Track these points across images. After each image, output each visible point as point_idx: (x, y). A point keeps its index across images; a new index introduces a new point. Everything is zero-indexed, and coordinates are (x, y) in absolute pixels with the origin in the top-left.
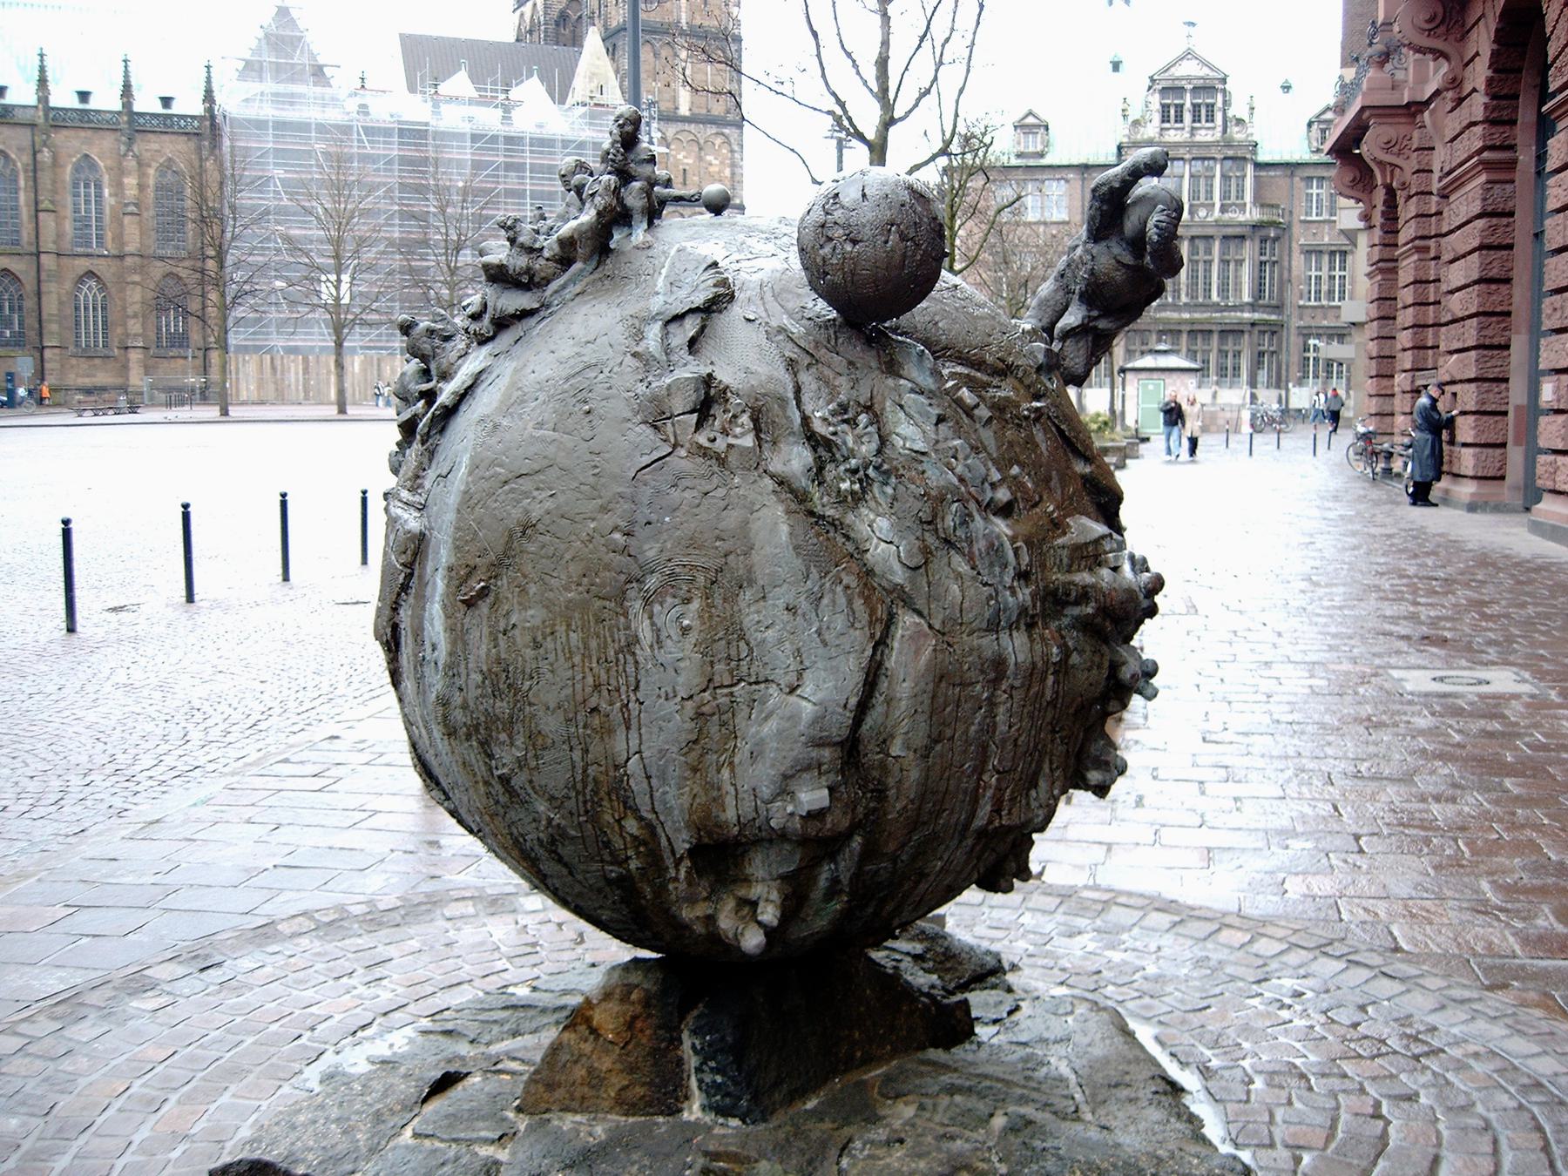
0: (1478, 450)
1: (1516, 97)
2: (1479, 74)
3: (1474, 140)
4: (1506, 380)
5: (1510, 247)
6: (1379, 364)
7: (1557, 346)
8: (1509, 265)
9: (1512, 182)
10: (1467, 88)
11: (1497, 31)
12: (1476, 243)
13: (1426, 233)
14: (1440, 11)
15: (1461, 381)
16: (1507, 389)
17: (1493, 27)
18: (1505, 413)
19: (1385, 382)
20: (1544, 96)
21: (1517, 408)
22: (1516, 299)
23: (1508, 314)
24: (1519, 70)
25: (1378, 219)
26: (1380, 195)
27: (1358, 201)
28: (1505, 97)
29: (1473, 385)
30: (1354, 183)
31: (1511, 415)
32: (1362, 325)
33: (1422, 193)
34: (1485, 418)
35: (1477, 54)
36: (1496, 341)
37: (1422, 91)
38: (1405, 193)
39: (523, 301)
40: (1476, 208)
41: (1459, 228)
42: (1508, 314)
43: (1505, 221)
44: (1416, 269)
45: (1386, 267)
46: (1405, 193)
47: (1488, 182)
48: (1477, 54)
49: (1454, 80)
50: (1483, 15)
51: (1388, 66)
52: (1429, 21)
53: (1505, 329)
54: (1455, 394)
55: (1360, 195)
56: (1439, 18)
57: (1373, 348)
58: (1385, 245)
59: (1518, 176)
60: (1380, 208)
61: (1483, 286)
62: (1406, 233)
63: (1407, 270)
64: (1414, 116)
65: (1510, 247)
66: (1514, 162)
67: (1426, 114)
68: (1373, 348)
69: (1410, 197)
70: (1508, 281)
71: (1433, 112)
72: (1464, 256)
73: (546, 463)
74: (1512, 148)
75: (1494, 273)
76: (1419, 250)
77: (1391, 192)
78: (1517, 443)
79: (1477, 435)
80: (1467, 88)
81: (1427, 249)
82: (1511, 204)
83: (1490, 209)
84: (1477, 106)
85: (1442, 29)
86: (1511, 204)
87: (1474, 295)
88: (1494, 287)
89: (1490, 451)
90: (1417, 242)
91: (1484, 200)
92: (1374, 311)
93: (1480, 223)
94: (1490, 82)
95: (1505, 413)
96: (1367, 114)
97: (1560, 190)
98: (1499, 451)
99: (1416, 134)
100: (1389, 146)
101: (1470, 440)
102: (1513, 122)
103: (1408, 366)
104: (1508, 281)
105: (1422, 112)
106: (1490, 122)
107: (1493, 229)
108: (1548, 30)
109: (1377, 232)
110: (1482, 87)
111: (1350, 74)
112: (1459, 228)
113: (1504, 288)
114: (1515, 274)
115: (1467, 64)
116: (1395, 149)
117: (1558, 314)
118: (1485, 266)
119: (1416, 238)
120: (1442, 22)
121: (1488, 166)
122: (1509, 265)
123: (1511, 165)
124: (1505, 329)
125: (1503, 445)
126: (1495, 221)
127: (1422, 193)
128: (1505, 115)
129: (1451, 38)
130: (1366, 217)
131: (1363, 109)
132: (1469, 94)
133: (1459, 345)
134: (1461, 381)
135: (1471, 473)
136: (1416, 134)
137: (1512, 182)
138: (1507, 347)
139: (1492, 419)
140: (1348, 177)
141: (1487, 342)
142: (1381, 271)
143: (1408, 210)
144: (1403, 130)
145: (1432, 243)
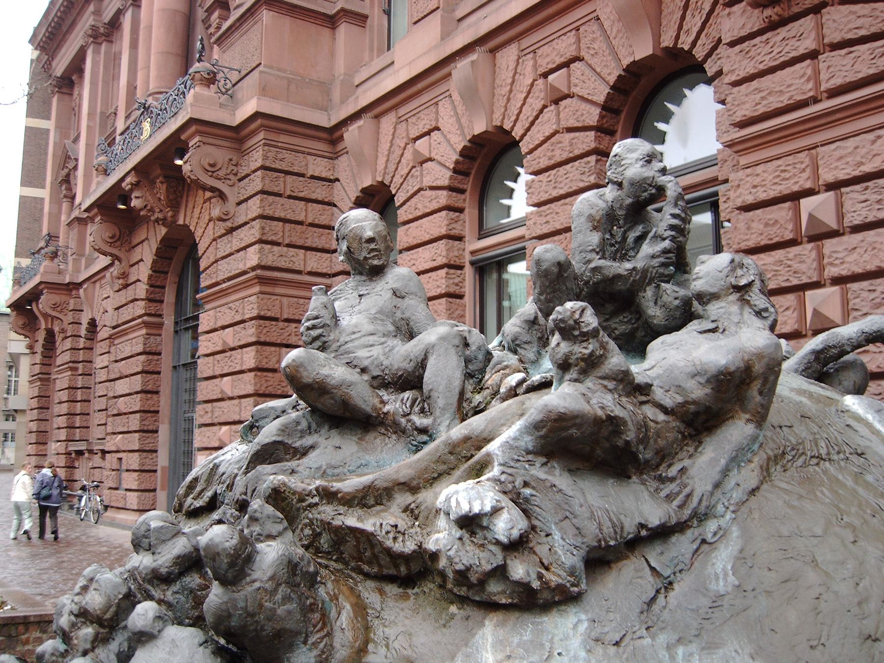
0: (140, 493)
1: (164, 287)
2: (143, 272)
3: (139, 308)
4: (156, 451)
5: (159, 373)
6: (37, 436)
7: (208, 434)
8: (158, 383)
9: (160, 335)
10: (132, 279)
11: (158, 248)
12: (139, 369)
13: (76, 359)
14: (118, 234)
15: (124, 451)
16: (157, 457)
17: (154, 247)
18: (155, 471)
19: (41, 447)
20: (197, 290)
21: (163, 468)
22: (162, 403)
23: (157, 412)
24: (167, 273)
25: (39, 348)
26: (41, 336)
27: (26, 336)
28: (158, 287)
29: (137, 454)
30: (24, 327)
31: (159, 472)
32: (23, 411)
33: (75, 336)
34: (144, 474)
35: (142, 260)
36: (150, 428)
37: (78, 277)
38: (62, 335)
39: (638, 504)
40: (140, 348)
41: (122, 359)
42: (157, 412)
43: (156, 357)
44: (70, 380)
45: (43, 378)
46: (62, 335)
47: (147, 334)
48: (142, 260)
49: (124, 273)
50: (147, 239)
51: (56, 260)
52: (111, 238)
53: (155, 421)
54: (120, 459)
55: (28, 334)
56: (117, 237)
57: (34, 426)
58: (43, 364)
59: (163, 333)
60: (41, 341)
61: (144, 395)
62: (62, 358)
63: (62, 380)
64: (71, 290)
65: (159, 373)
66: (162, 324)
67: (81, 291)
68: (34, 426)
69: (67, 337)
70: (157, 393)
71: (85, 290)
72: (127, 376)
73: (448, 625)
74: (160, 316)
75: (150, 387)
76: (71, 369)
77: (50, 334)
78: (163, 489)
79: (139, 485)
80: (132, 279)
81: (76, 369)
82: (159, 348)
83: (148, 350)
84: (141, 290)
85: (119, 243)
86: (159, 348)
87: (139, 399)
88: (149, 396)
89: (147, 494)
90: (71, 364)
91: (145, 344)
92: (34, 403)
93: (142, 358)
94: (150, 277)
95: (155, 471)
96: (43, 286)
97: (210, 344)
98: (152, 494)
99: (72, 301)
100: (55, 307)
101: (134, 487)
102: (162, 302)
103: (64, 438)
104: (157, 393)
105: (78, 289)
106: (149, 300)
107: (149, 362)
108: (200, 253)
109: (38, 358)
110: (146, 280)
111: (26, 262)
112: (122, 359)
113: (155, 397)
114: (161, 389)
115: (132, 265)
116: (59, 309)
117: (210, 415)
118: (144, 383)
119: (70, 362)
120: (118, 240)
121: (146, 324)
122: (158, 383)
123: (160, 326)
124: (155, 421)
125: (154, 490)
126: (150, 357)
127: (75, 336)
128: (157, 297)
129: (123, 249)
130: (30, 347)
131: (41, 283)
132: (135, 282)
133: (125, 429)
134: (124, 451)
135: (136, 508)
136: (72, 301)
137: (160, 335)
138: (156, 431)
139: (148, 475)
140: (21, 323)
141: (146, 428)
142: (40, 379)
143: (63, 345)
144: (64, 298)
145: (80, 366)
